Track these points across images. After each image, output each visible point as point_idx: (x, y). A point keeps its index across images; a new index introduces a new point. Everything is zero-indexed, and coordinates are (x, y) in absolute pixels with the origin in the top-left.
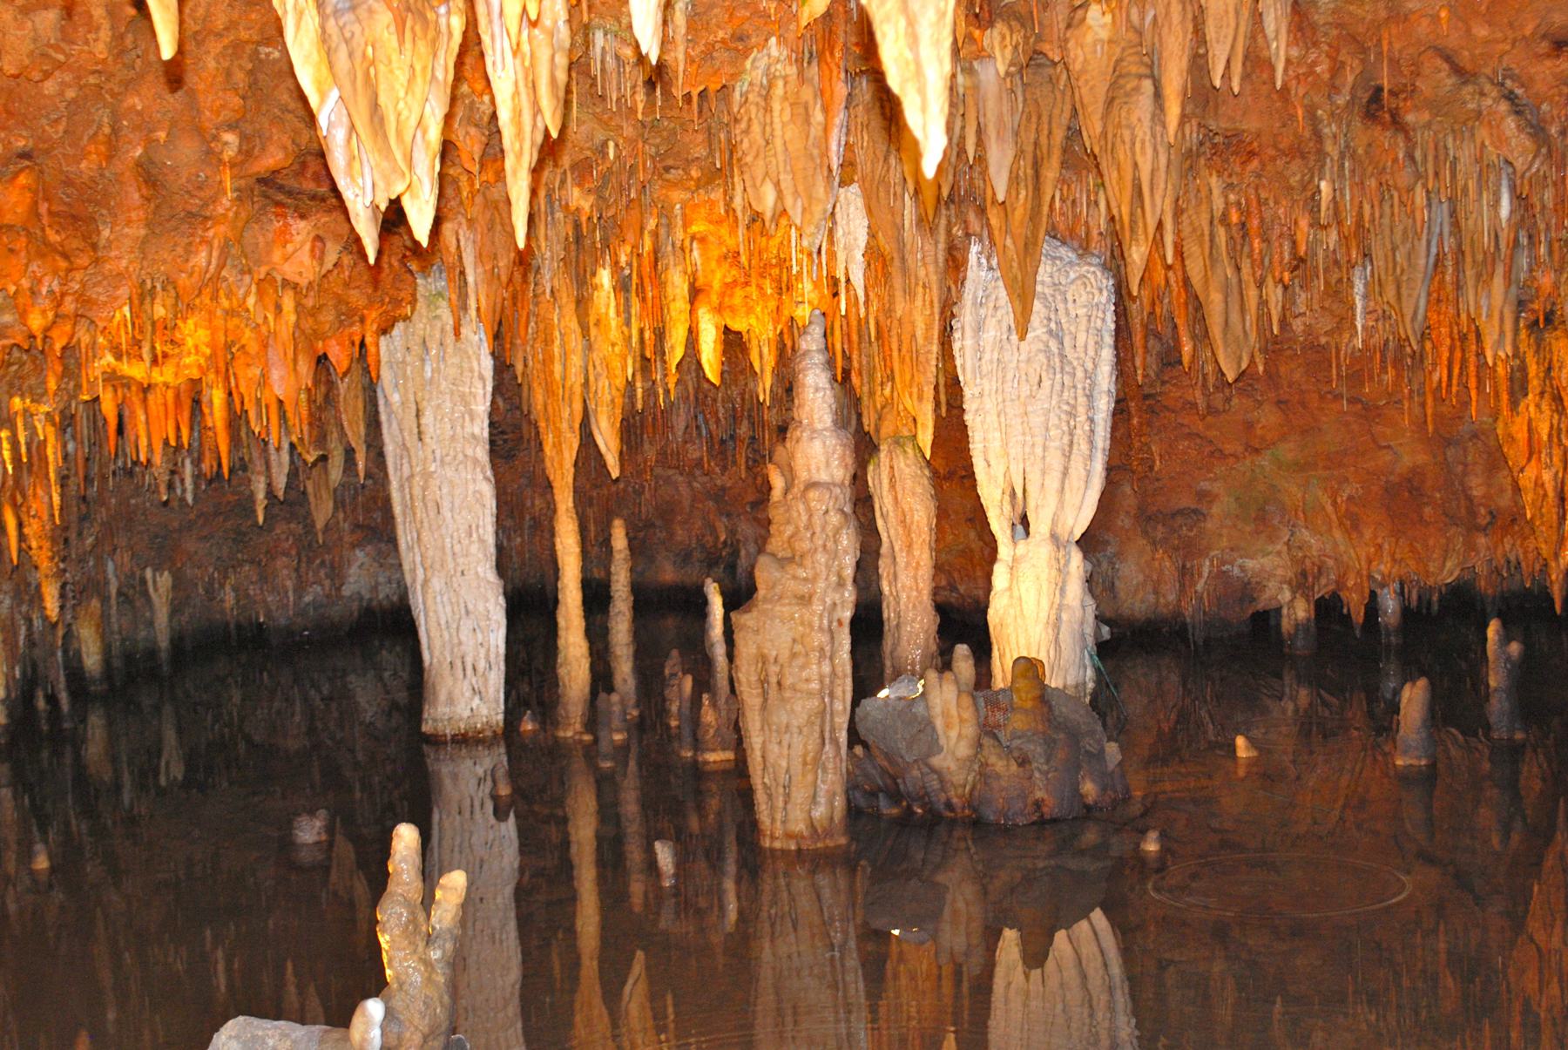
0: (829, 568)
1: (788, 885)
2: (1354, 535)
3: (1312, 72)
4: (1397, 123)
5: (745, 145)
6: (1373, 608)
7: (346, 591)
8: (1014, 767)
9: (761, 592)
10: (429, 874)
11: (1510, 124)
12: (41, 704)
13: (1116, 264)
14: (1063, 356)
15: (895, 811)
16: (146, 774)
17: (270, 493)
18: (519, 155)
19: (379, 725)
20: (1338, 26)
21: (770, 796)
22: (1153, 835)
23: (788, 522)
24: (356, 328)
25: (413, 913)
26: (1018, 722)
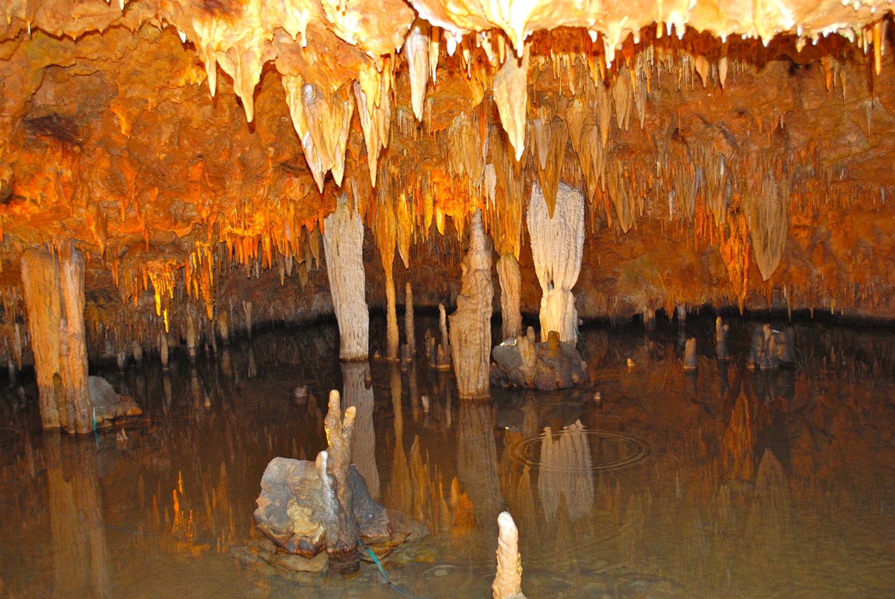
3: (653, 123)
4: (684, 141)
7: (313, 309)
8: (549, 370)
9: (459, 308)
10: (343, 408)
11: (724, 141)
12: (207, 348)
13: (584, 191)
14: (566, 224)
17: (286, 275)
18: (373, 154)
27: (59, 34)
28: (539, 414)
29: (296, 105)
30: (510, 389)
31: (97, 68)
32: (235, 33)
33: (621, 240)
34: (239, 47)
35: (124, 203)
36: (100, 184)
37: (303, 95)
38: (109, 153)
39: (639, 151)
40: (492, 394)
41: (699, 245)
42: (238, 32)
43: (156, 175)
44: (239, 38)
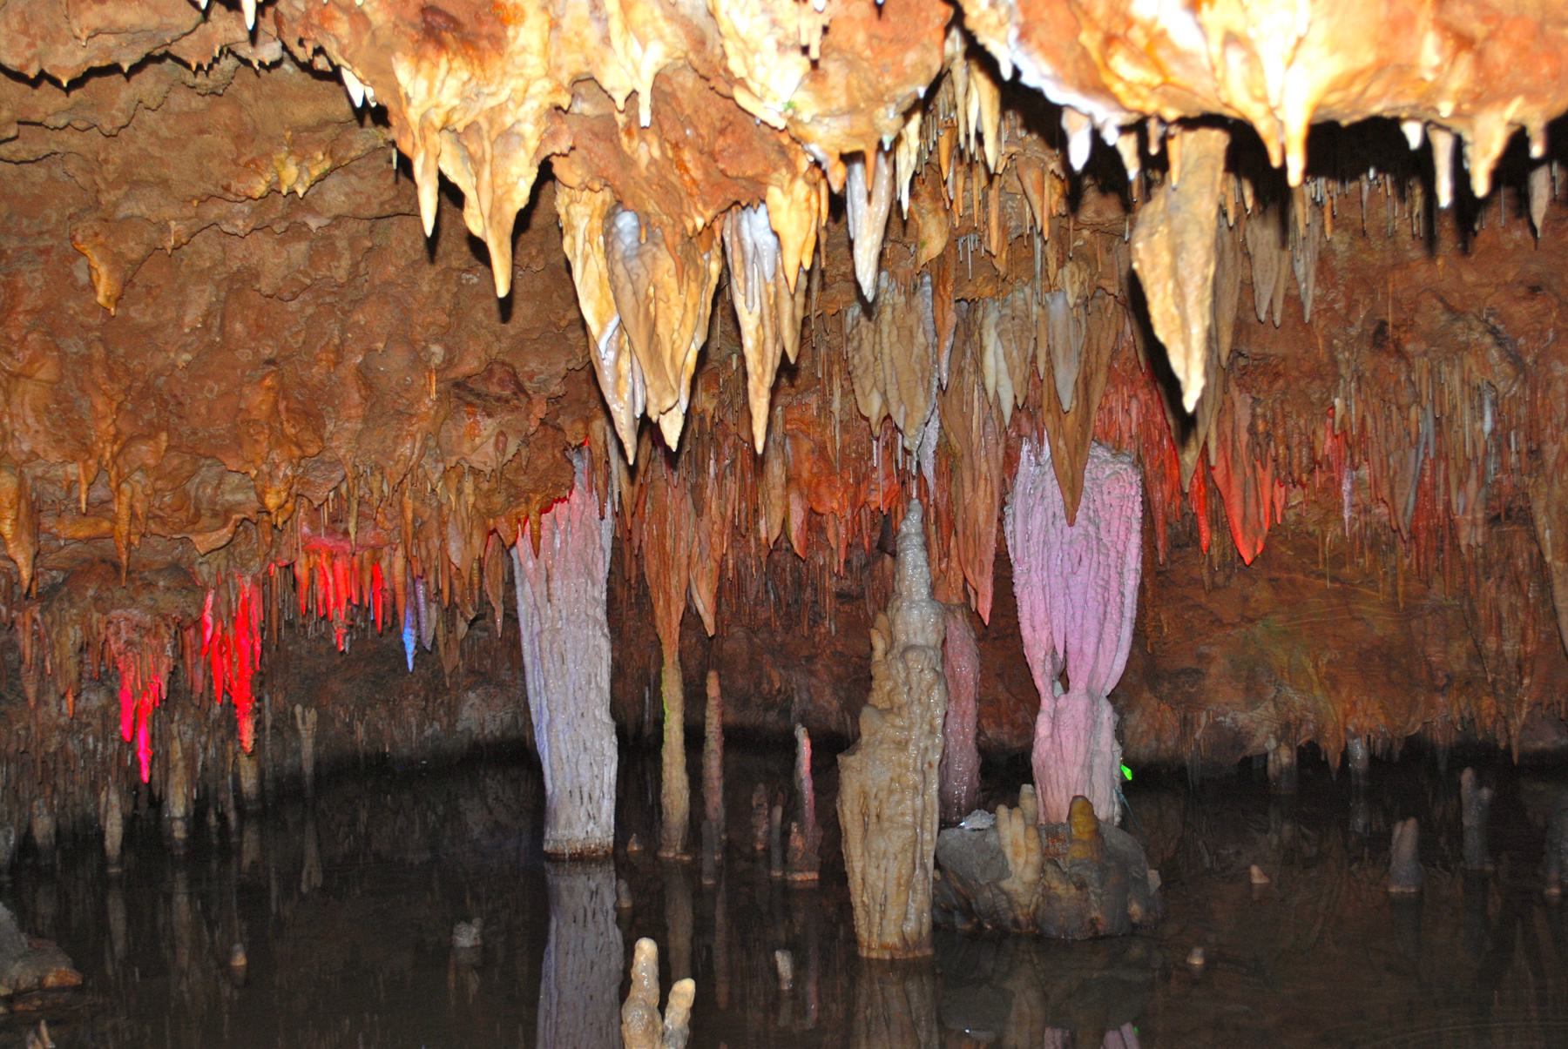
0: (922, 717)
1: (882, 989)
2: (1333, 693)
3: (1331, 309)
4: (1400, 352)
5: (856, 361)
6: (1346, 756)
8: (1073, 891)
9: (865, 738)
10: (666, 982)
11: (1494, 353)
12: (212, 820)
14: (1099, 540)
15: (968, 927)
16: (290, 881)
18: (761, 380)
19: (484, 842)
20: (1352, 271)
21: (868, 913)
22: (1198, 951)
23: (888, 678)
24: (522, 508)
25: (652, 1015)
26: (1077, 852)
27: (32, 73)
28: (1046, 996)
29: (586, 258)
30: (976, 935)
31: (53, 147)
32: (486, 90)
33: (1220, 579)
34: (491, 122)
35: (86, 468)
36: (30, 421)
37: (609, 232)
38: (57, 348)
39: (1295, 373)
40: (935, 944)
41: (1407, 595)
42: (493, 88)
43: (163, 404)
44: (492, 102)
